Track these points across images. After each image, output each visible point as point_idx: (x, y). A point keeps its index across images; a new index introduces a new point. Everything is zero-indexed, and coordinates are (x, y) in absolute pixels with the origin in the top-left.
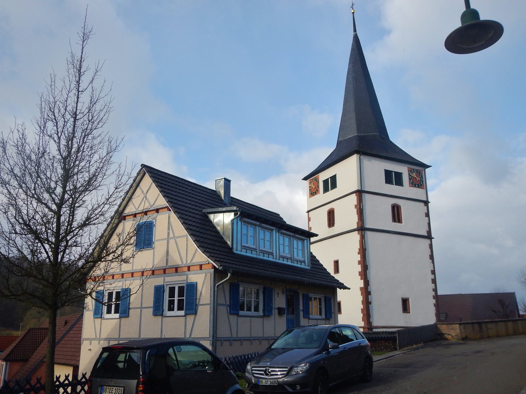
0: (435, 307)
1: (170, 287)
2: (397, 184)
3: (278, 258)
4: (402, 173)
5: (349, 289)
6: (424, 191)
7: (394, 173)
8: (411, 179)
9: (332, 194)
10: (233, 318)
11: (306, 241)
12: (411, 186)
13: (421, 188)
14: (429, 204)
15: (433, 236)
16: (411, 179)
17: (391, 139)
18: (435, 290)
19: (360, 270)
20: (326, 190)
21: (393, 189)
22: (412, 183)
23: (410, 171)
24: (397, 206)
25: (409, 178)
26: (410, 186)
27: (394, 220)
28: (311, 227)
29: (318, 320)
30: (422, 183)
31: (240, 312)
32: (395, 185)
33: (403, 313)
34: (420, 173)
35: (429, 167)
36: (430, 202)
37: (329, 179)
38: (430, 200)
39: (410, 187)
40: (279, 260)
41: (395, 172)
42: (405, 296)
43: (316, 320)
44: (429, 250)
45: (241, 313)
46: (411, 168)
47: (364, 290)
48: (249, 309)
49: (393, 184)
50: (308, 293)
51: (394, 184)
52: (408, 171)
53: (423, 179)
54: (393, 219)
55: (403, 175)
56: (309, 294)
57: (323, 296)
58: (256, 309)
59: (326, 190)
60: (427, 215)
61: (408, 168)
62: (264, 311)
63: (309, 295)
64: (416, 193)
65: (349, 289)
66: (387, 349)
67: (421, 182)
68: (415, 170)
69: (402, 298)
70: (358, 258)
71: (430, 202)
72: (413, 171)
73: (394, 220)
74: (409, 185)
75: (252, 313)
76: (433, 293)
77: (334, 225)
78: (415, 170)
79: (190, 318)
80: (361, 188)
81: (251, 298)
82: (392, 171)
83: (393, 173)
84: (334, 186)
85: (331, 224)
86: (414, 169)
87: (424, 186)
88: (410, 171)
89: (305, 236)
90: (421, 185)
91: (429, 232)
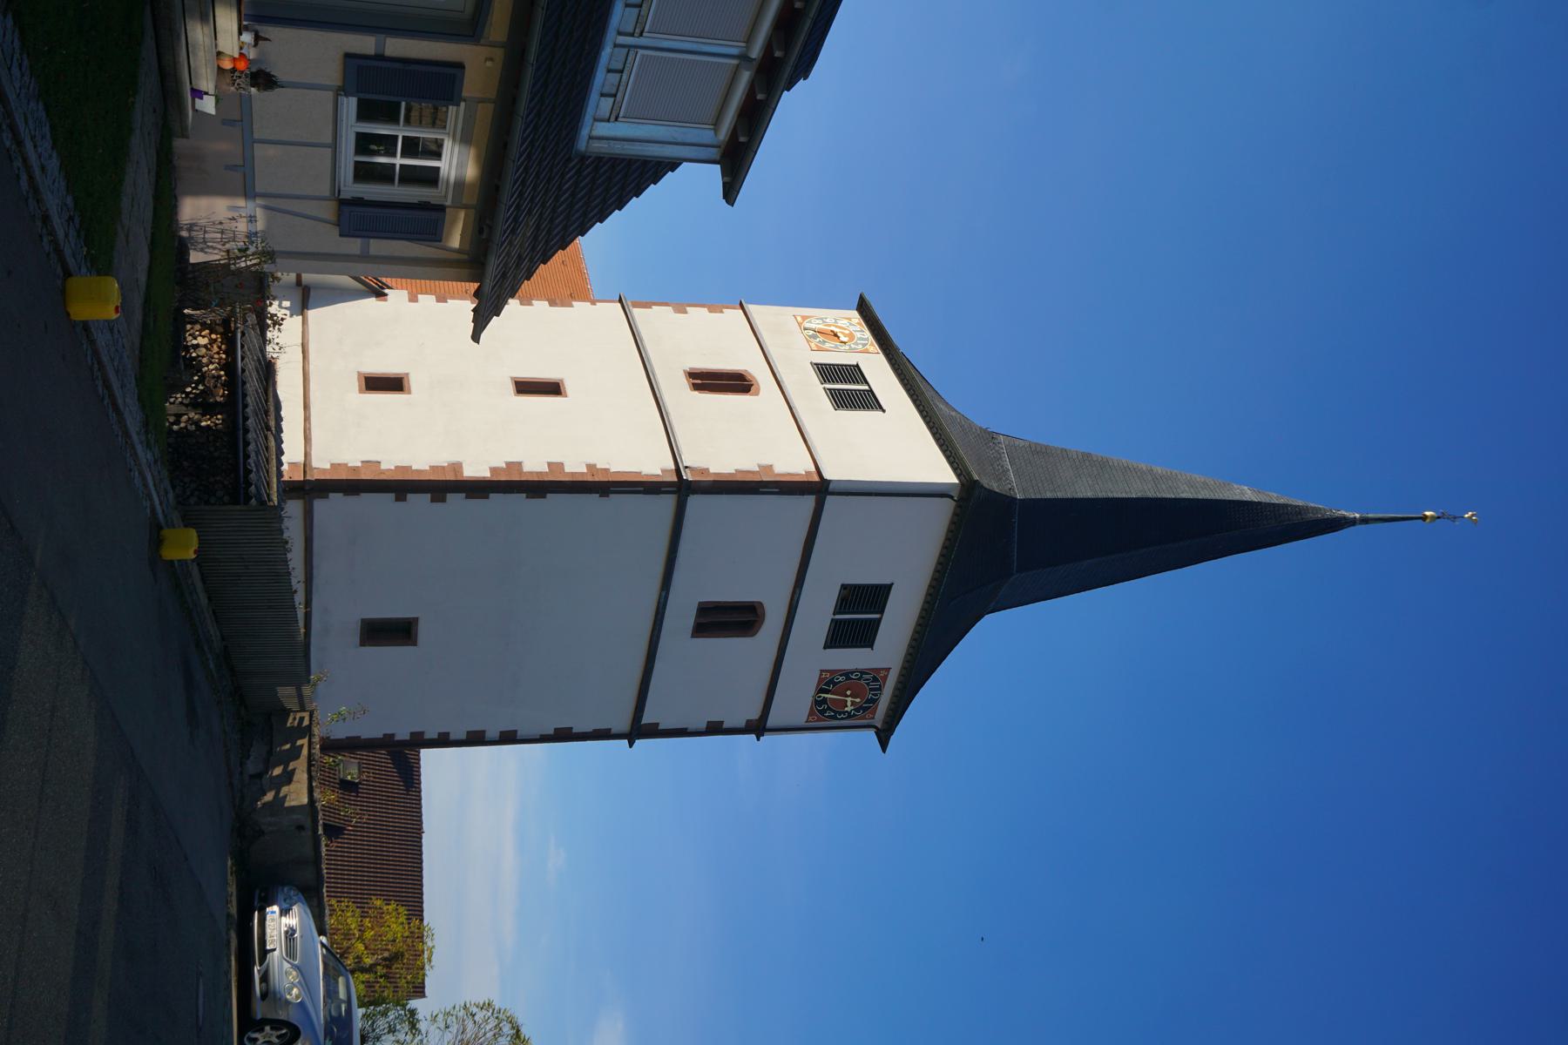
0: (382, 737)
1: (408, 137)
2: (836, 625)
3: (622, 40)
4: (871, 646)
5: (476, 337)
6: (801, 720)
7: (875, 619)
8: (848, 678)
9: (813, 396)
10: (332, 73)
11: (707, 135)
12: (821, 675)
13: (811, 713)
14: (753, 736)
15: (638, 742)
16: (848, 678)
17: (989, 619)
18: (443, 741)
19: (527, 468)
20: (827, 372)
21: (818, 611)
22: (831, 682)
23: (875, 677)
24: (755, 621)
25: (852, 673)
26: (822, 671)
27: (705, 610)
28: (686, 312)
29: (329, 151)
30: (827, 717)
31: (353, 101)
32: (832, 620)
33: (363, 621)
34: (865, 709)
35: (884, 745)
36: (758, 739)
37: (867, 388)
38: (766, 738)
39: (818, 673)
40: (616, 46)
41: (879, 620)
42: (423, 631)
43: (329, 140)
44: (588, 728)
45: (350, 105)
46: (885, 678)
47: (450, 477)
48: (365, 143)
49: (834, 614)
50: (465, 100)
51: (838, 617)
52: (878, 670)
53: (842, 719)
54: (711, 606)
55: (868, 650)
56: (463, 104)
57: (446, 197)
58: (364, 173)
59: (827, 372)
60: (715, 729)
61: (888, 670)
62: (358, 202)
63: (458, 105)
64: (796, 698)
65: (476, 337)
66: (197, 493)
67: (834, 711)
68: (876, 695)
69: (416, 620)
70: (575, 466)
71: (758, 739)
72: (874, 685)
73: (705, 610)
74: (826, 671)
75: (348, 157)
76: (431, 734)
77: (695, 390)
78: (876, 695)
79: (328, 210)
80: (833, 493)
81: (408, 121)
82: (882, 612)
83: (877, 616)
84: (842, 401)
85: (699, 382)
86: (880, 689)
87: (817, 721)
88: (874, 678)
89: (734, 134)
90: (822, 712)
91: (654, 732)
